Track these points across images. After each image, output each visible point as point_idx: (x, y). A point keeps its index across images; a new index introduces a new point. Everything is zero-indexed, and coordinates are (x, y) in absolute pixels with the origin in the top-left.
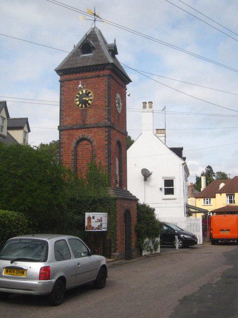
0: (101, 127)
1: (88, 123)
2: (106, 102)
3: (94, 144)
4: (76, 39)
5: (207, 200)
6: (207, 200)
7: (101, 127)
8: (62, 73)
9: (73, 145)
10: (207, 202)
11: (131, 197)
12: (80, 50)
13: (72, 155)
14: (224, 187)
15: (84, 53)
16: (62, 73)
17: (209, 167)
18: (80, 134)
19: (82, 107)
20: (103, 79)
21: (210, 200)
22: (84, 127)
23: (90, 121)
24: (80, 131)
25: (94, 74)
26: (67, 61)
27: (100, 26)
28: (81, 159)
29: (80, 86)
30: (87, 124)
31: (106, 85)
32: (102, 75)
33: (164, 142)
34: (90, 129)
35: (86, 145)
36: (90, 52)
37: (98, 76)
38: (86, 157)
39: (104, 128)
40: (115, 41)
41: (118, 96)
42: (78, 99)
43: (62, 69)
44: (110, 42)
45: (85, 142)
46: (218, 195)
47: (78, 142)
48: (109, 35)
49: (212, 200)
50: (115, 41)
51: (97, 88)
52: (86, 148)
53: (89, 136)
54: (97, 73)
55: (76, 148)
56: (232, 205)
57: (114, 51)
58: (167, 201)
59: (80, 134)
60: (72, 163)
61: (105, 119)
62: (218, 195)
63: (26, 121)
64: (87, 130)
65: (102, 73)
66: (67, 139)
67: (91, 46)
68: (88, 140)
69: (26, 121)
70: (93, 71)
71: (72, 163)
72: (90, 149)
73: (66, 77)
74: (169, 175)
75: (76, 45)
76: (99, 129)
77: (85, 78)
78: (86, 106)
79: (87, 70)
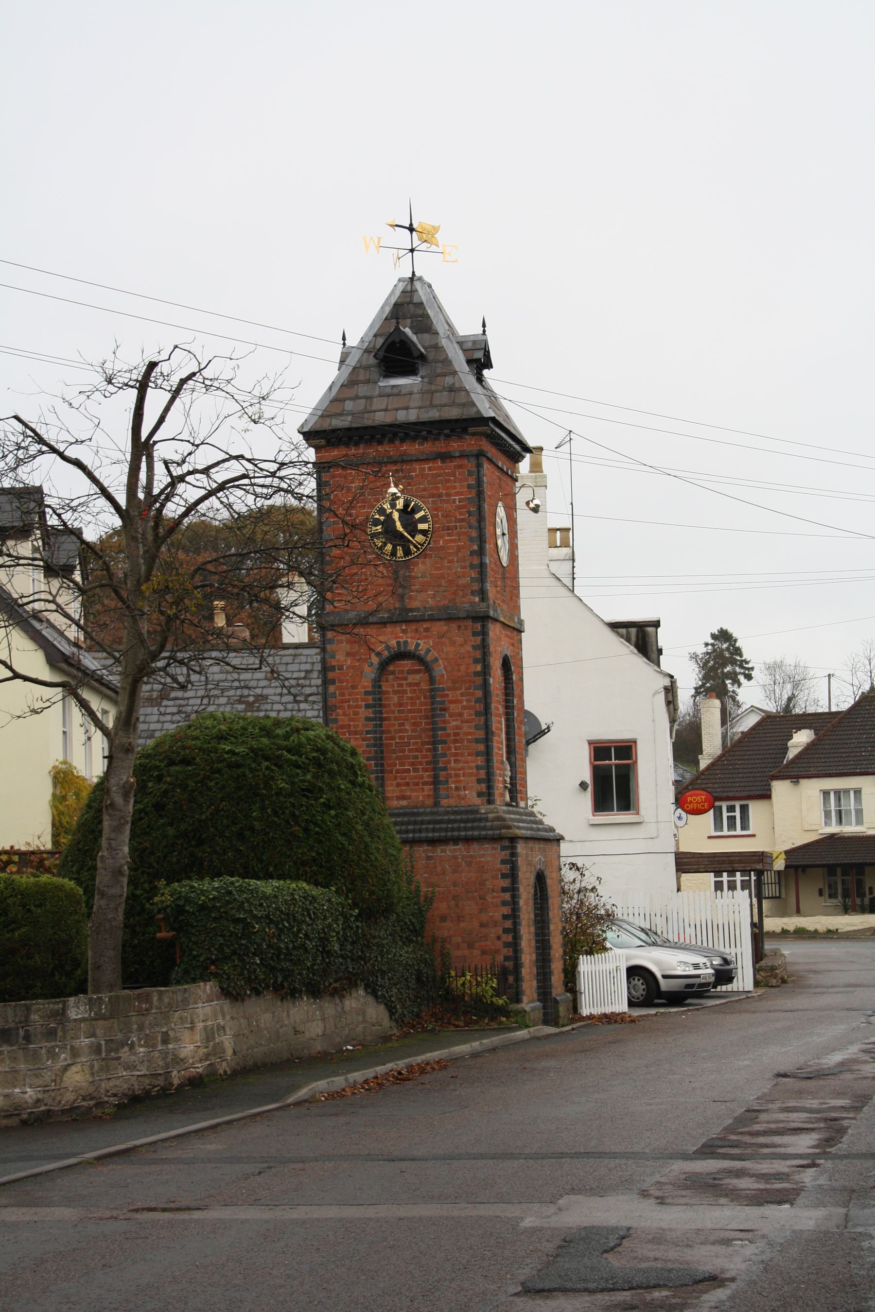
0: (459, 618)
1: (416, 604)
2: (471, 540)
3: (440, 669)
4: (359, 318)
5: (731, 809)
6: (731, 809)
7: (459, 618)
8: (323, 442)
9: (370, 673)
10: (732, 820)
11: (546, 830)
12: (372, 361)
13: (367, 706)
14: (809, 748)
15: (387, 376)
16: (323, 442)
17: (723, 636)
18: (390, 638)
19: (394, 553)
20: (460, 467)
21: (744, 809)
22: (403, 617)
23: (422, 600)
24: (389, 629)
25: (428, 447)
26: (334, 401)
27: (427, 267)
28: (396, 719)
29: (393, 490)
30: (412, 610)
31: (469, 486)
32: (457, 454)
33: (567, 581)
34: (426, 625)
35: (410, 672)
36: (410, 371)
37: (445, 457)
38: (410, 711)
39: (469, 623)
40: (484, 325)
41: (501, 512)
42: (379, 528)
43: (318, 428)
44: (466, 326)
45: (406, 665)
46: (780, 789)
47: (383, 666)
48: (461, 312)
49: (755, 809)
50: (484, 325)
51: (440, 495)
52: (410, 685)
53: (423, 645)
54: (440, 446)
55: (377, 683)
56: (850, 829)
57: (480, 361)
58: (603, 829)
59: (390, 638)
60: (368, 732)
61: (473, 593)
62: (780, 789)
63: (600, 751)
64: (413, 626)
65: (455, 446)
66: (348, 654)
67: (416, 354)
68: (420, 660)
69: (600, 751)
70: (425, 439)
71: (368, 732)
72: (425, 686)
73: (335, 453)
74: (613, 731)
75: (353, 341)
76: (454, 625)
77: (403, 461)
78: (407, 552)
79: (407, 435)
